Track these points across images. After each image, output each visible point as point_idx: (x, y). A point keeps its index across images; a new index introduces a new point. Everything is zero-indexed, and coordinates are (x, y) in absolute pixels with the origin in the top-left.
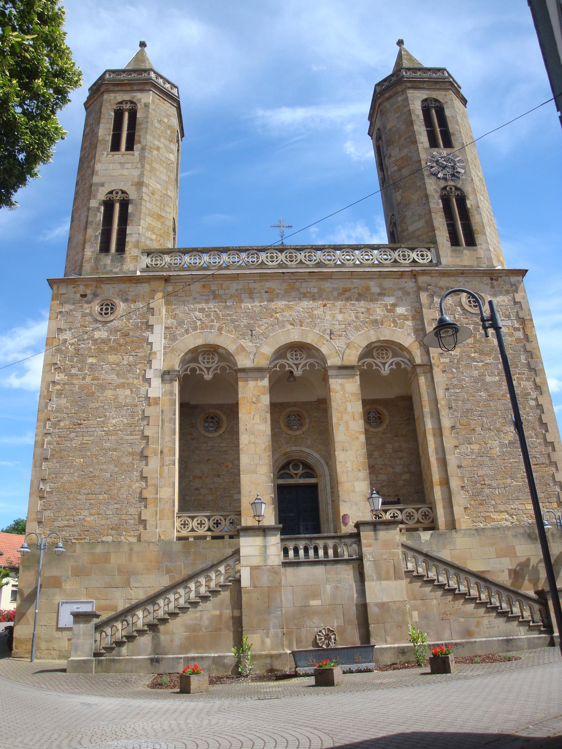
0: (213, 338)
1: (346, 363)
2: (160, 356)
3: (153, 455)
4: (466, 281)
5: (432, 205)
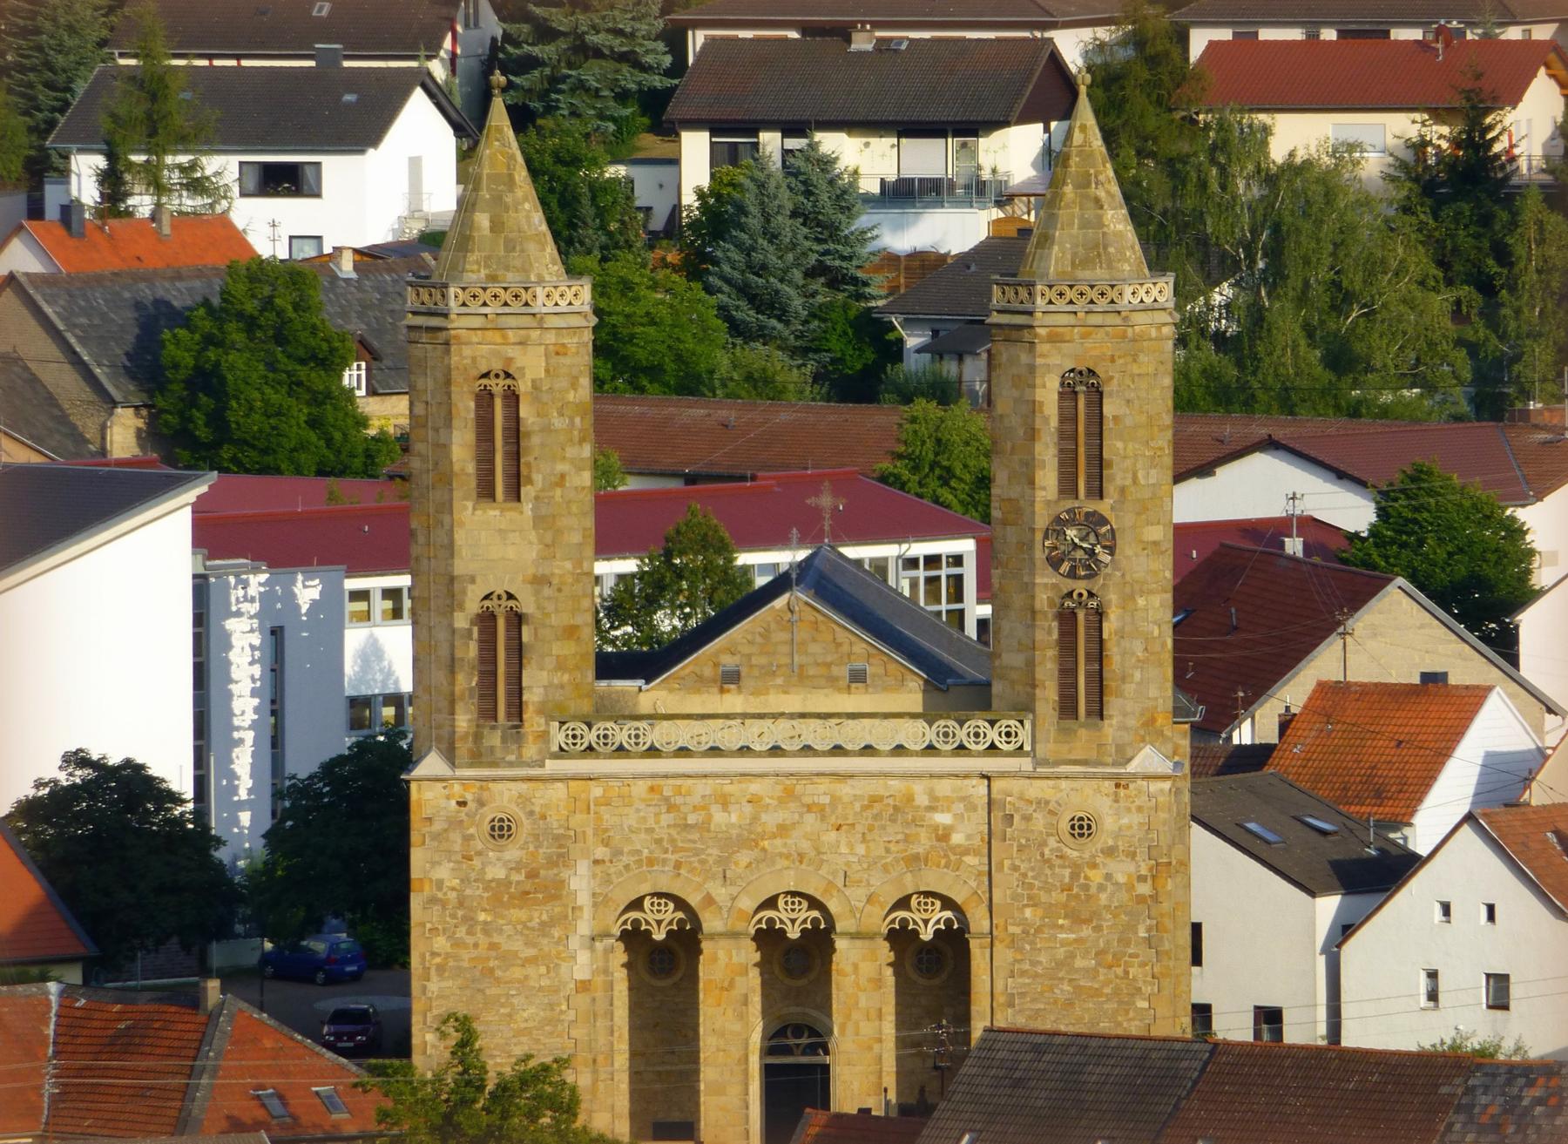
2: (587, 913)
5: (1040, 636)
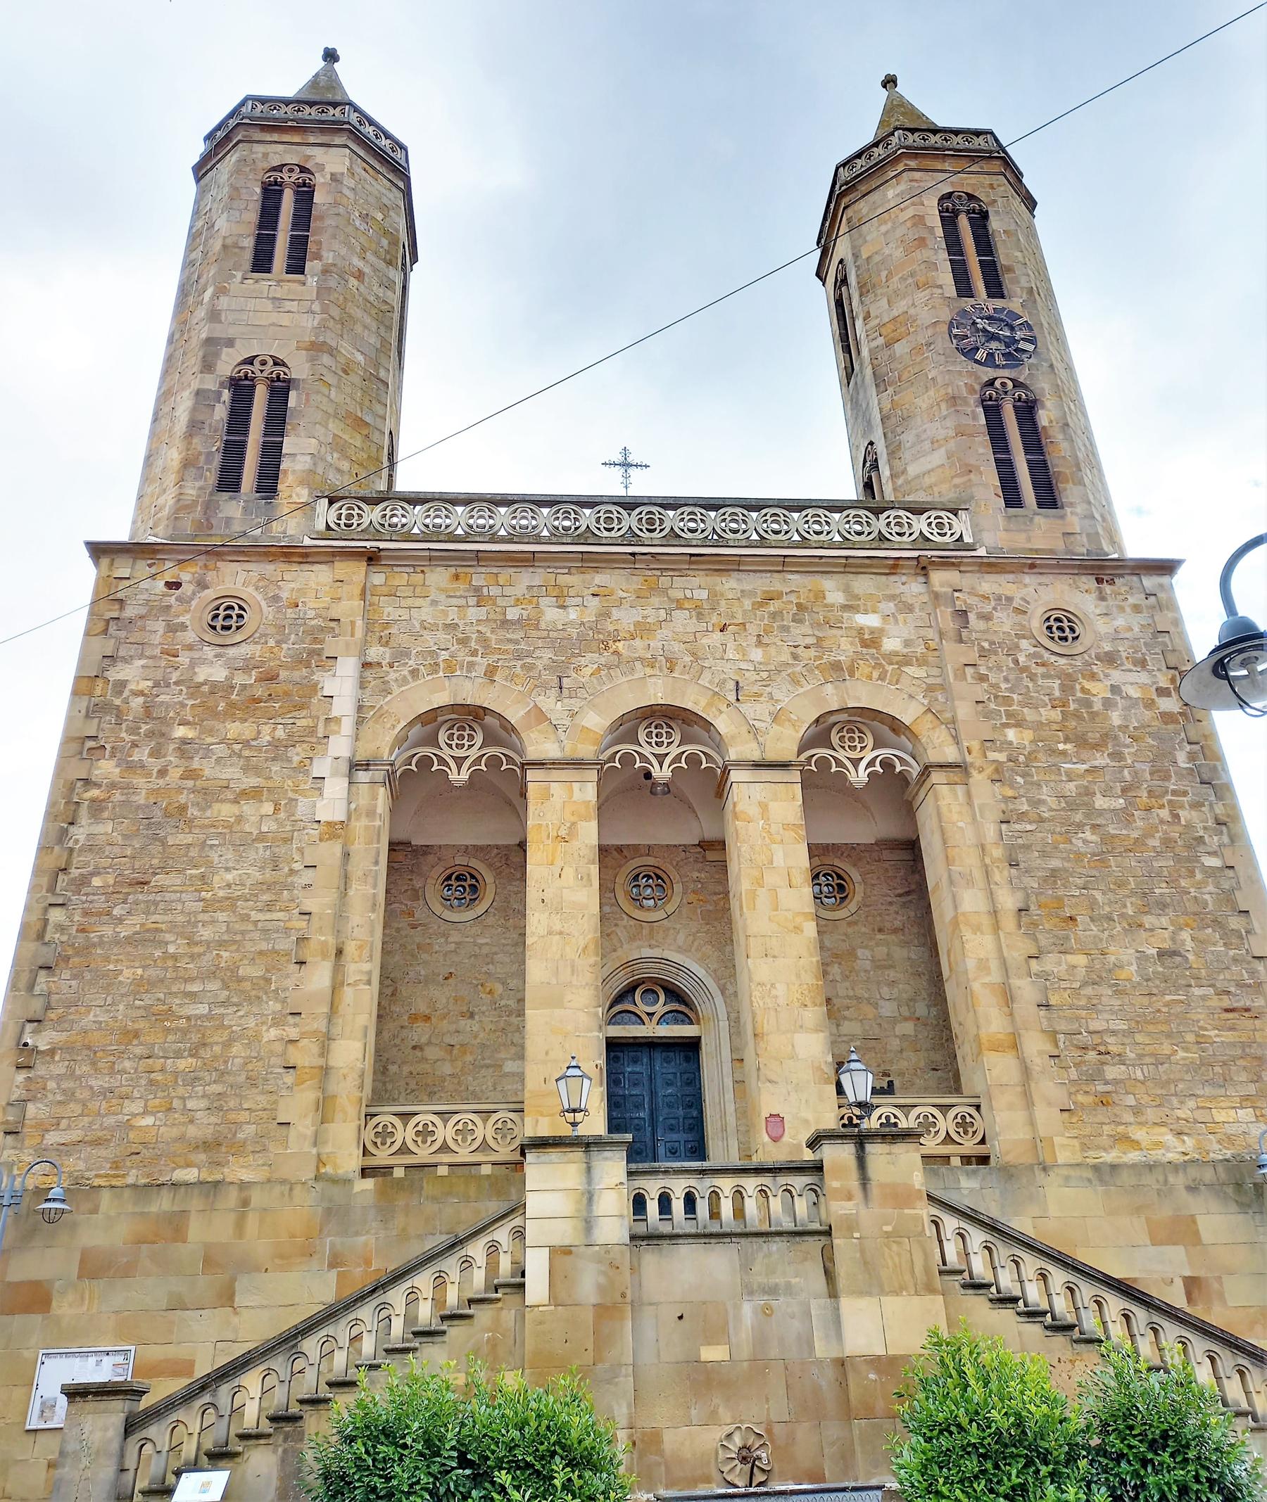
0: (471, 692)
1: (771, 756)
2: (347, 726)
3: (319, 958)
4: (1040, 584)
